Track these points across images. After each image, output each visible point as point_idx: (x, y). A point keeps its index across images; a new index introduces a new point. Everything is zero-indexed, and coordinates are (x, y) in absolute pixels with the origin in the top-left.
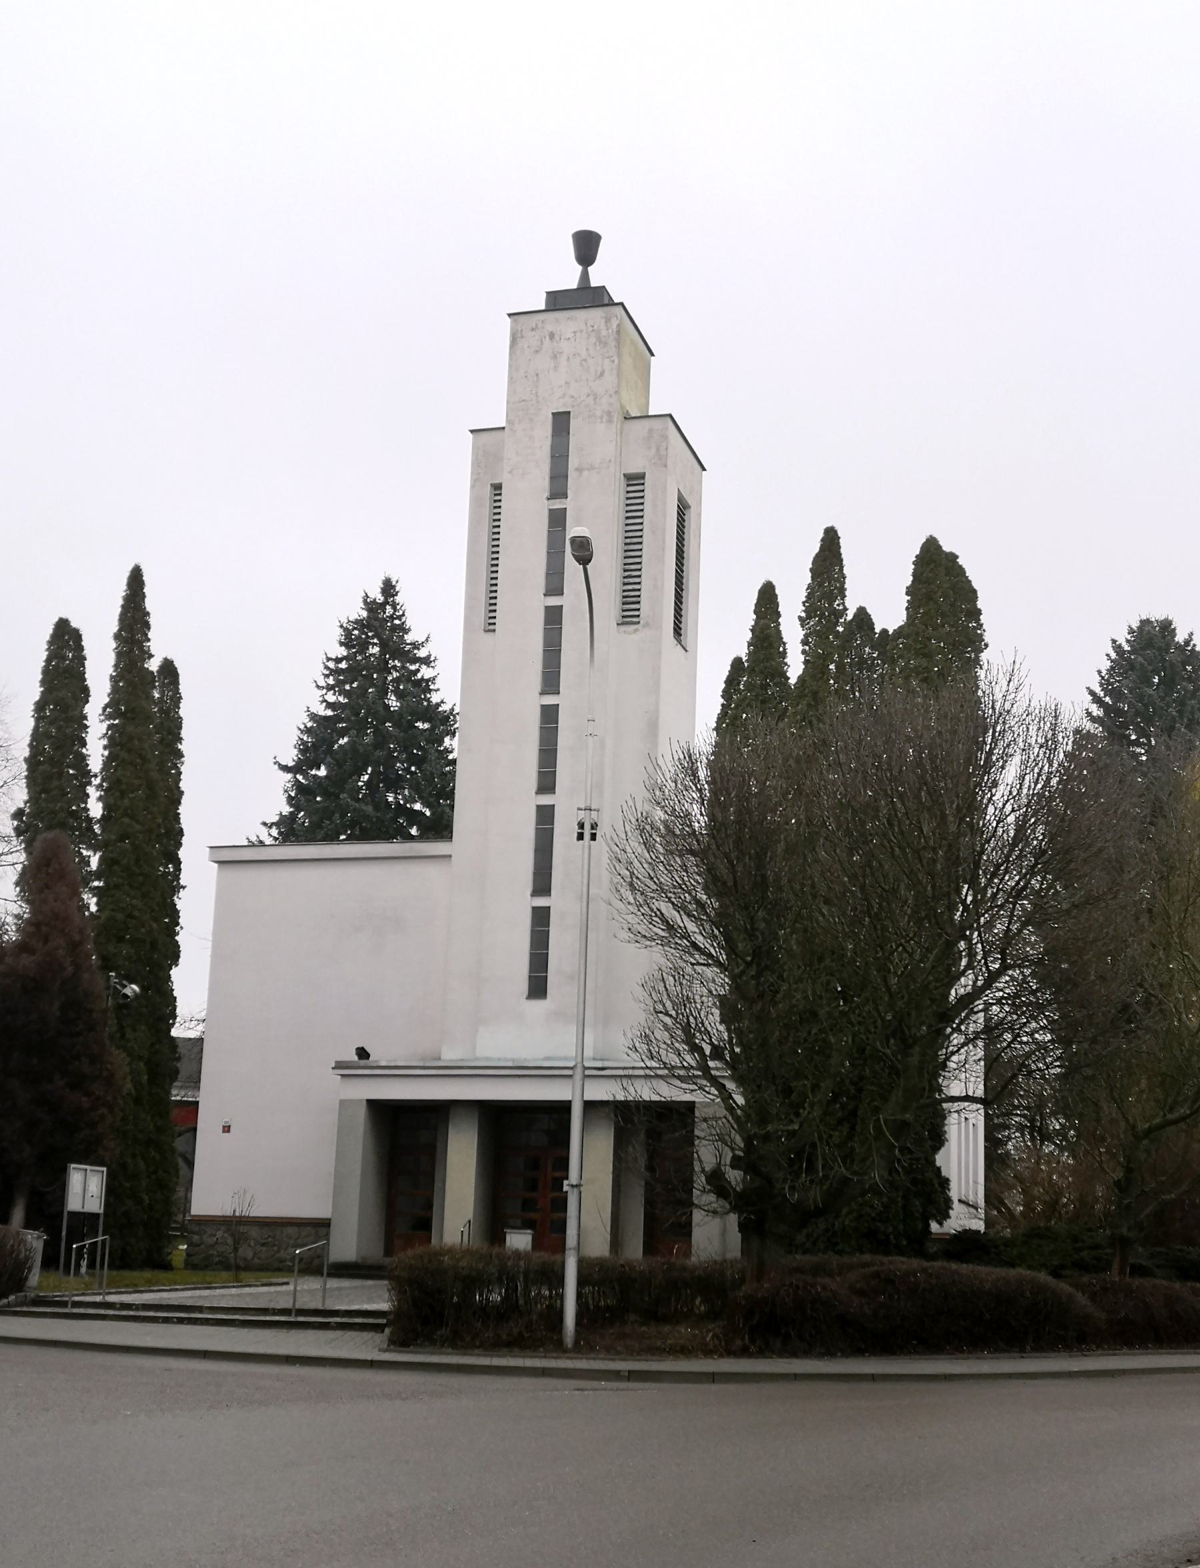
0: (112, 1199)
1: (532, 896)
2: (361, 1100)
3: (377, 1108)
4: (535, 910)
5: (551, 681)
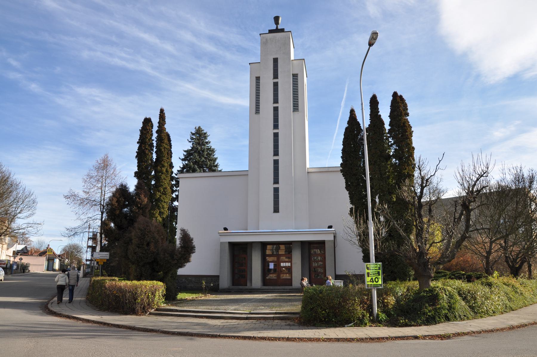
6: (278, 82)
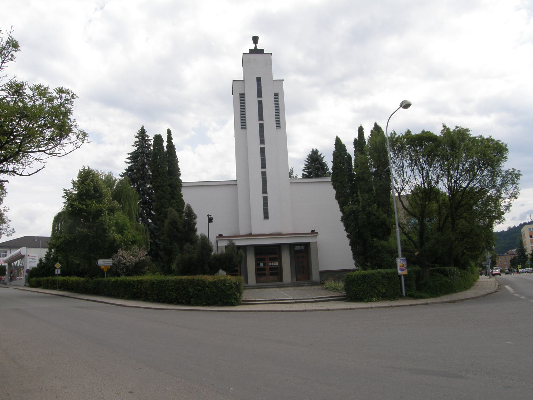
6: (267, 197)
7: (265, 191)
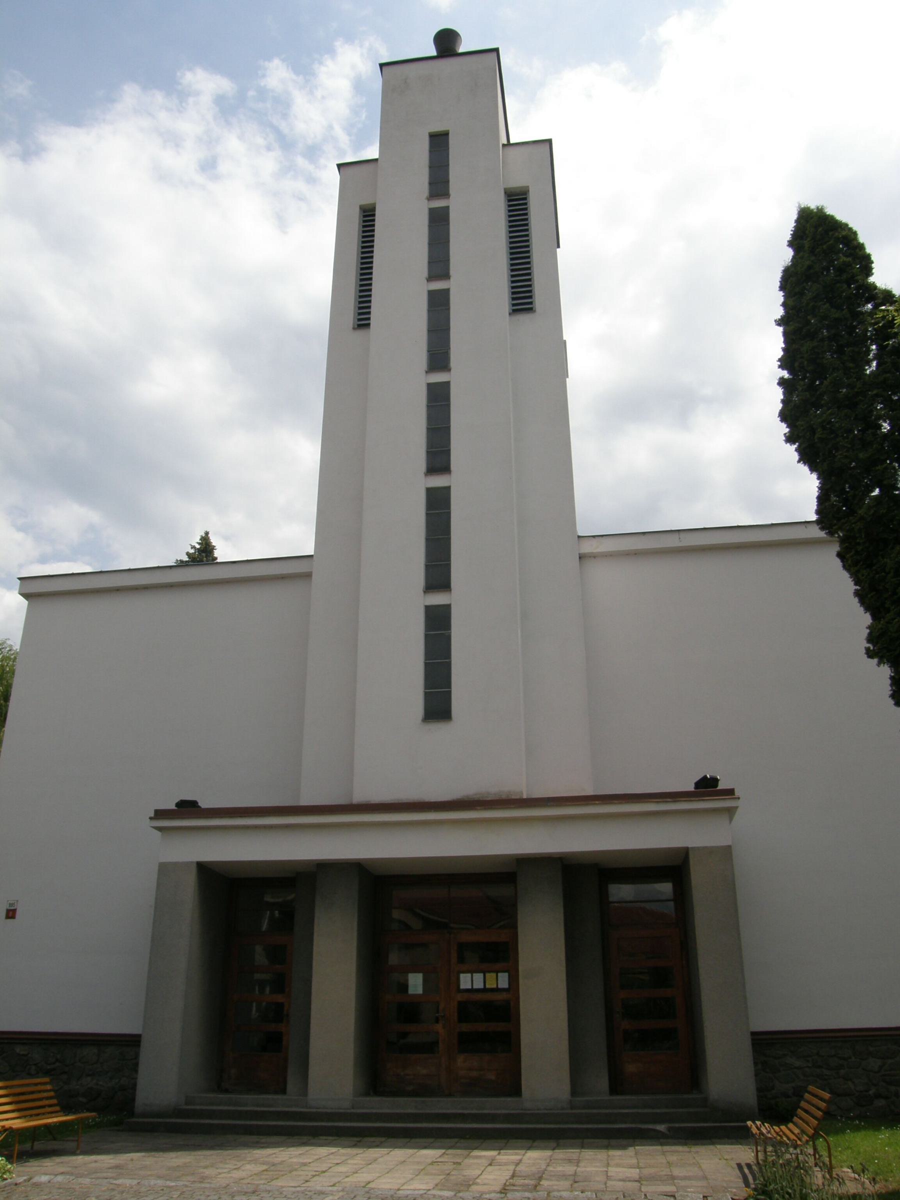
0: (78, 1152)
1: (425, 592)
2: (187, 864)
3: (208, 873)
4: (429, 610)
5: (439, 358)
6: (448, 607)
7: (438, 575)
